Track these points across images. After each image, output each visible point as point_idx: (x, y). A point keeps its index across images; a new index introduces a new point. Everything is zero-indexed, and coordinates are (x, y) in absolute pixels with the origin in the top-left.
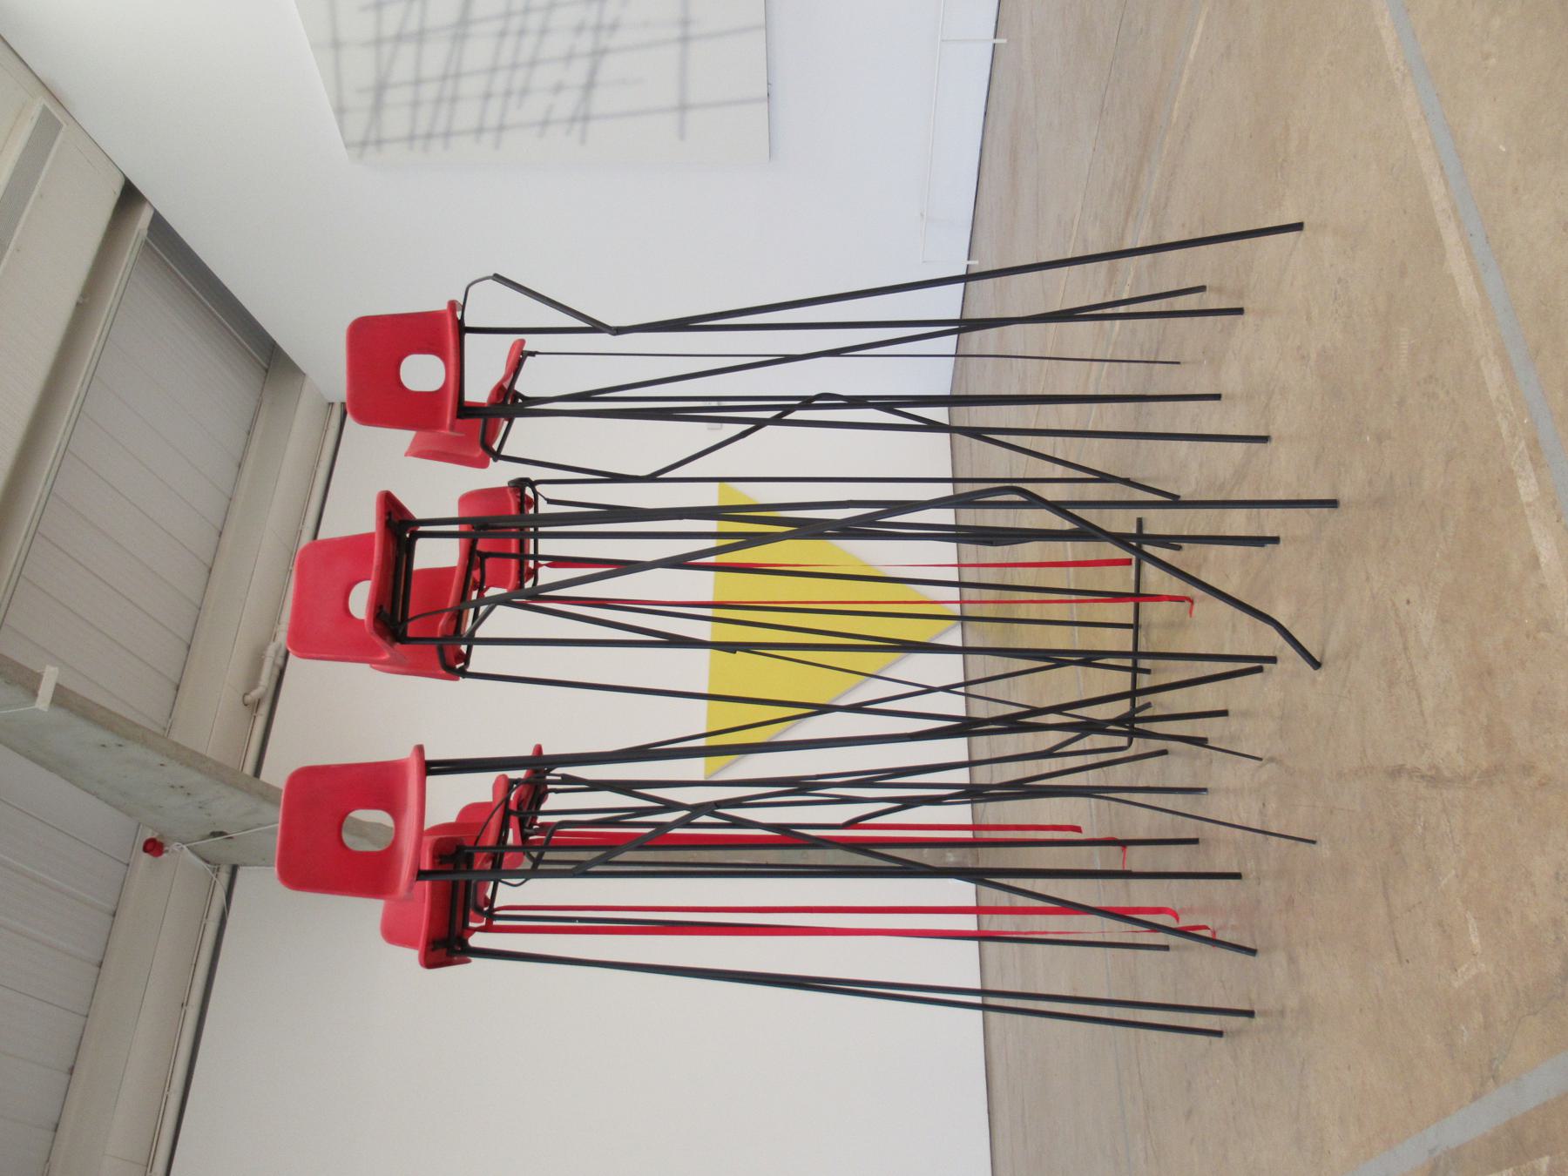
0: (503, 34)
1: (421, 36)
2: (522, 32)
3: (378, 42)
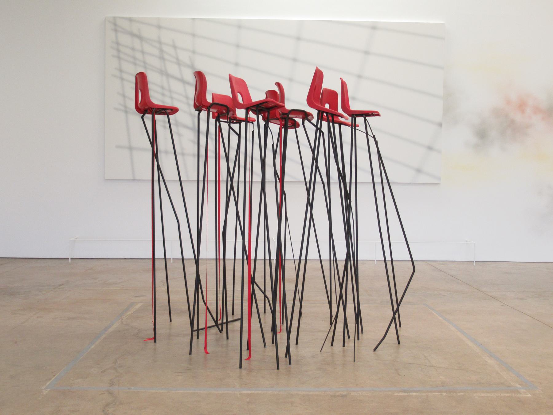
0: (163, 88)
1: (162, 58)
2: (163, 95)
3: (160, 43)
